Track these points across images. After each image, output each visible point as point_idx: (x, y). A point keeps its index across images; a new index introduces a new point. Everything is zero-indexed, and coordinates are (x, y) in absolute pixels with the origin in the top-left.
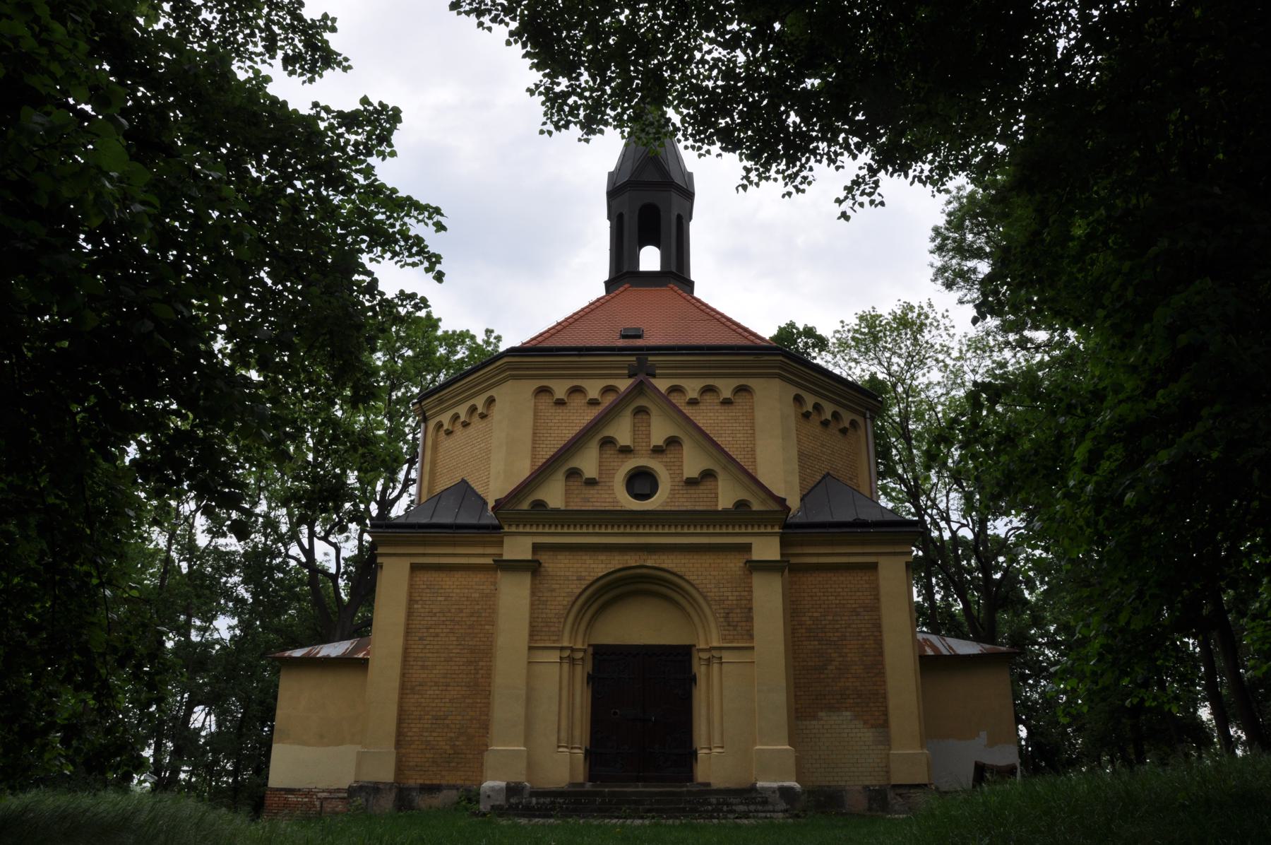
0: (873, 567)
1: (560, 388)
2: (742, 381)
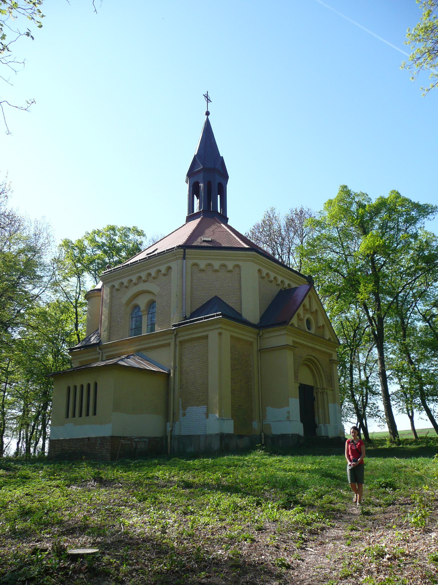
0: (206, 337)
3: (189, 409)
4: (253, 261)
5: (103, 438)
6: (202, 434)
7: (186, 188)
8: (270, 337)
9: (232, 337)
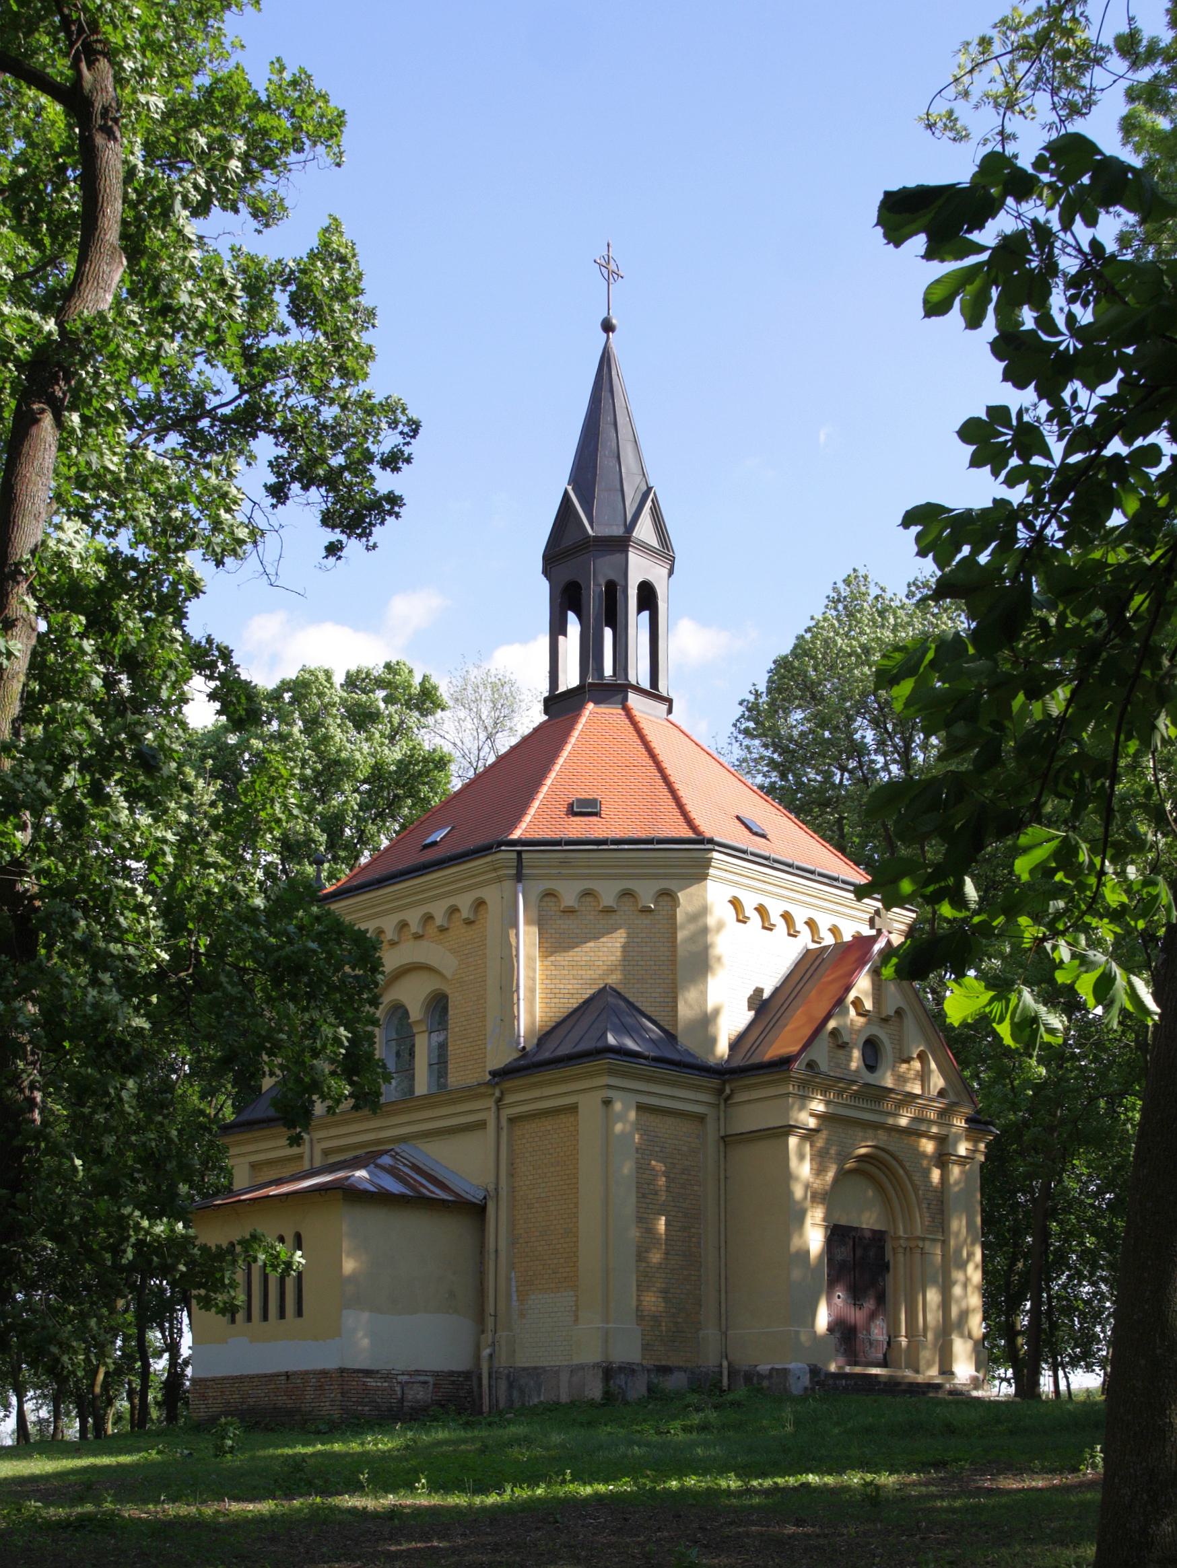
0: (573, 1109)
1: (569, 893)
5: (324, 1373)
6: (566, 1363)
7: (541, 589)
8: (749, 1101)
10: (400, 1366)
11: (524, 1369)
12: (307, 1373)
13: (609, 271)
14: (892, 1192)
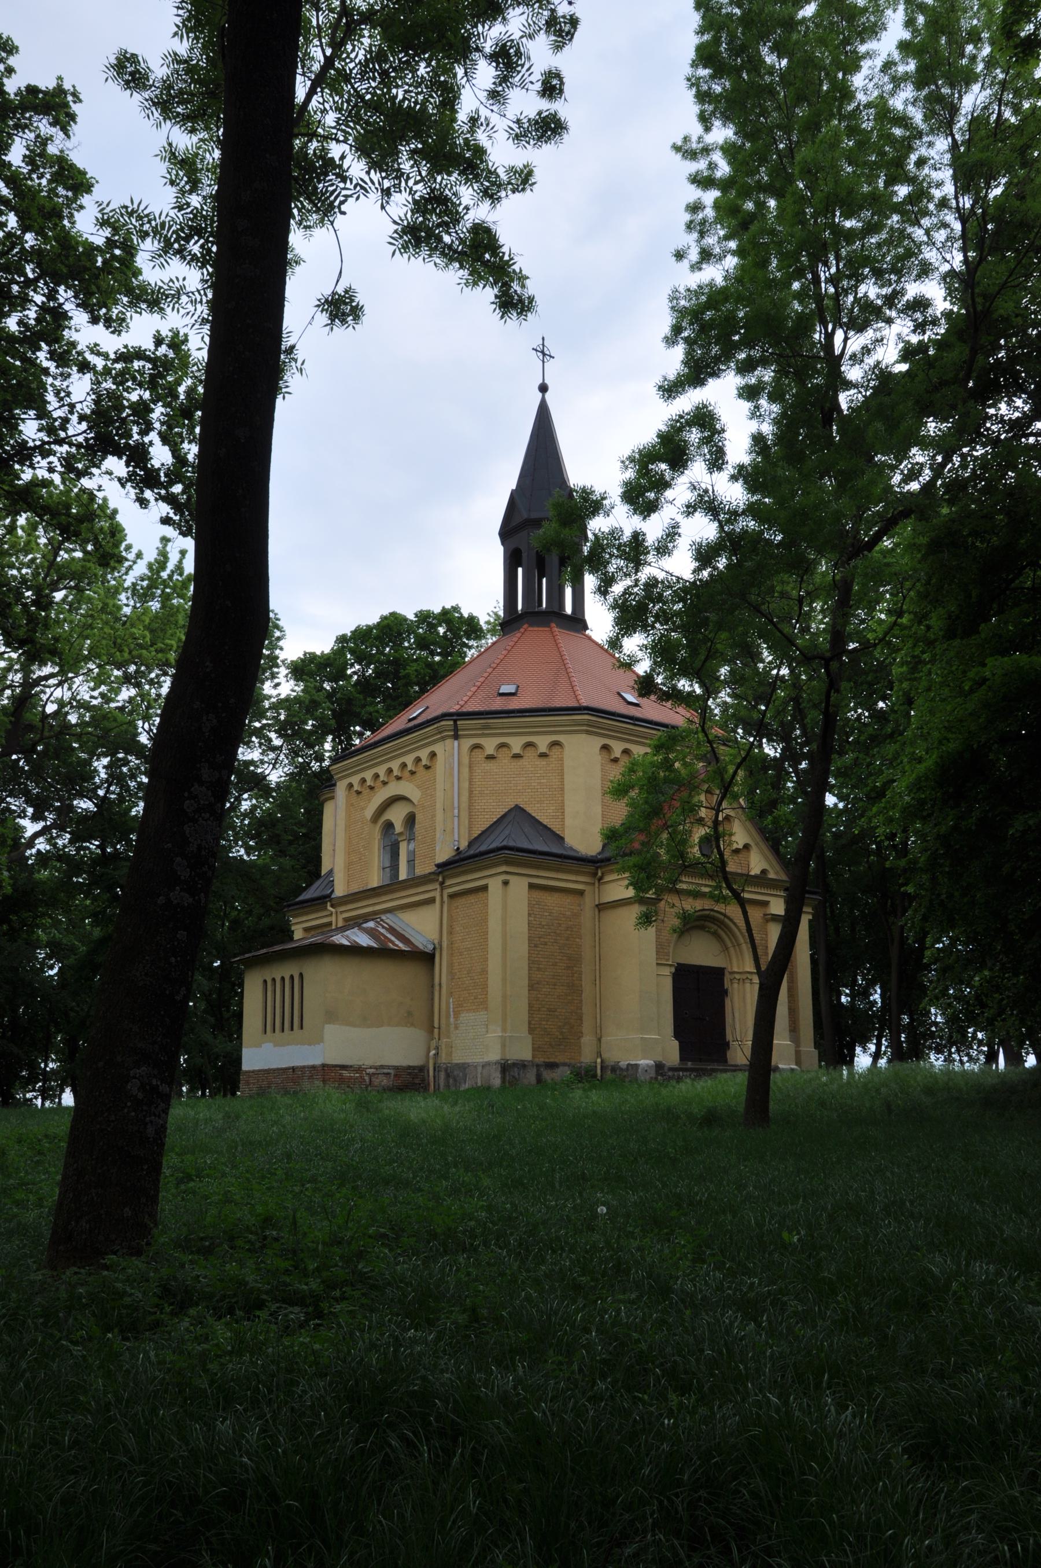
0: (485, 888)
1: (490, 745)
2: (554, 738)
3: (465, 1017)
4: (588, 732)
5: (313, 1067)
9: (532, 886)
10: (369, 1062)
11: (457, 1064)
12: (304, 1067)
13: (544, 353)
14: (729, 944)
